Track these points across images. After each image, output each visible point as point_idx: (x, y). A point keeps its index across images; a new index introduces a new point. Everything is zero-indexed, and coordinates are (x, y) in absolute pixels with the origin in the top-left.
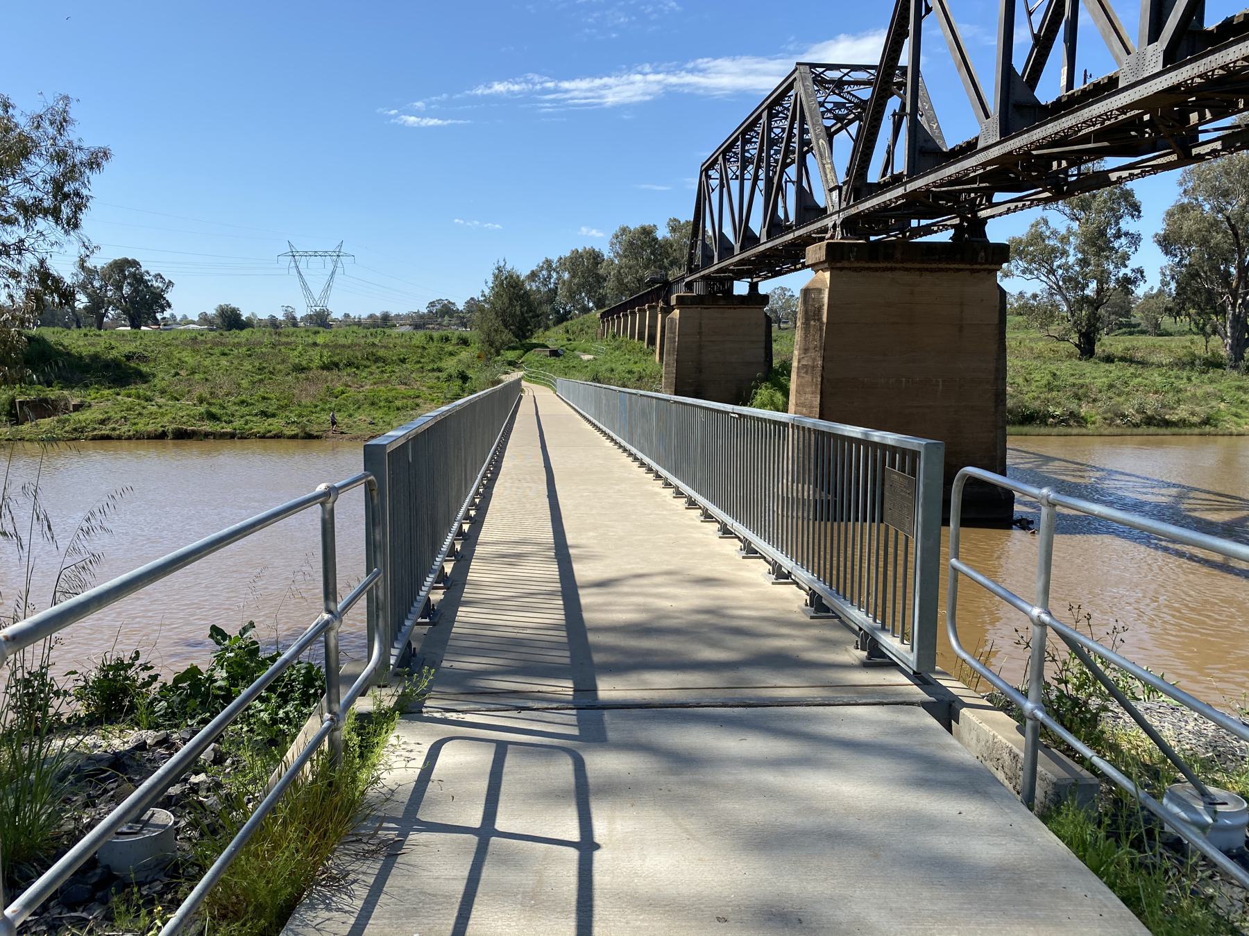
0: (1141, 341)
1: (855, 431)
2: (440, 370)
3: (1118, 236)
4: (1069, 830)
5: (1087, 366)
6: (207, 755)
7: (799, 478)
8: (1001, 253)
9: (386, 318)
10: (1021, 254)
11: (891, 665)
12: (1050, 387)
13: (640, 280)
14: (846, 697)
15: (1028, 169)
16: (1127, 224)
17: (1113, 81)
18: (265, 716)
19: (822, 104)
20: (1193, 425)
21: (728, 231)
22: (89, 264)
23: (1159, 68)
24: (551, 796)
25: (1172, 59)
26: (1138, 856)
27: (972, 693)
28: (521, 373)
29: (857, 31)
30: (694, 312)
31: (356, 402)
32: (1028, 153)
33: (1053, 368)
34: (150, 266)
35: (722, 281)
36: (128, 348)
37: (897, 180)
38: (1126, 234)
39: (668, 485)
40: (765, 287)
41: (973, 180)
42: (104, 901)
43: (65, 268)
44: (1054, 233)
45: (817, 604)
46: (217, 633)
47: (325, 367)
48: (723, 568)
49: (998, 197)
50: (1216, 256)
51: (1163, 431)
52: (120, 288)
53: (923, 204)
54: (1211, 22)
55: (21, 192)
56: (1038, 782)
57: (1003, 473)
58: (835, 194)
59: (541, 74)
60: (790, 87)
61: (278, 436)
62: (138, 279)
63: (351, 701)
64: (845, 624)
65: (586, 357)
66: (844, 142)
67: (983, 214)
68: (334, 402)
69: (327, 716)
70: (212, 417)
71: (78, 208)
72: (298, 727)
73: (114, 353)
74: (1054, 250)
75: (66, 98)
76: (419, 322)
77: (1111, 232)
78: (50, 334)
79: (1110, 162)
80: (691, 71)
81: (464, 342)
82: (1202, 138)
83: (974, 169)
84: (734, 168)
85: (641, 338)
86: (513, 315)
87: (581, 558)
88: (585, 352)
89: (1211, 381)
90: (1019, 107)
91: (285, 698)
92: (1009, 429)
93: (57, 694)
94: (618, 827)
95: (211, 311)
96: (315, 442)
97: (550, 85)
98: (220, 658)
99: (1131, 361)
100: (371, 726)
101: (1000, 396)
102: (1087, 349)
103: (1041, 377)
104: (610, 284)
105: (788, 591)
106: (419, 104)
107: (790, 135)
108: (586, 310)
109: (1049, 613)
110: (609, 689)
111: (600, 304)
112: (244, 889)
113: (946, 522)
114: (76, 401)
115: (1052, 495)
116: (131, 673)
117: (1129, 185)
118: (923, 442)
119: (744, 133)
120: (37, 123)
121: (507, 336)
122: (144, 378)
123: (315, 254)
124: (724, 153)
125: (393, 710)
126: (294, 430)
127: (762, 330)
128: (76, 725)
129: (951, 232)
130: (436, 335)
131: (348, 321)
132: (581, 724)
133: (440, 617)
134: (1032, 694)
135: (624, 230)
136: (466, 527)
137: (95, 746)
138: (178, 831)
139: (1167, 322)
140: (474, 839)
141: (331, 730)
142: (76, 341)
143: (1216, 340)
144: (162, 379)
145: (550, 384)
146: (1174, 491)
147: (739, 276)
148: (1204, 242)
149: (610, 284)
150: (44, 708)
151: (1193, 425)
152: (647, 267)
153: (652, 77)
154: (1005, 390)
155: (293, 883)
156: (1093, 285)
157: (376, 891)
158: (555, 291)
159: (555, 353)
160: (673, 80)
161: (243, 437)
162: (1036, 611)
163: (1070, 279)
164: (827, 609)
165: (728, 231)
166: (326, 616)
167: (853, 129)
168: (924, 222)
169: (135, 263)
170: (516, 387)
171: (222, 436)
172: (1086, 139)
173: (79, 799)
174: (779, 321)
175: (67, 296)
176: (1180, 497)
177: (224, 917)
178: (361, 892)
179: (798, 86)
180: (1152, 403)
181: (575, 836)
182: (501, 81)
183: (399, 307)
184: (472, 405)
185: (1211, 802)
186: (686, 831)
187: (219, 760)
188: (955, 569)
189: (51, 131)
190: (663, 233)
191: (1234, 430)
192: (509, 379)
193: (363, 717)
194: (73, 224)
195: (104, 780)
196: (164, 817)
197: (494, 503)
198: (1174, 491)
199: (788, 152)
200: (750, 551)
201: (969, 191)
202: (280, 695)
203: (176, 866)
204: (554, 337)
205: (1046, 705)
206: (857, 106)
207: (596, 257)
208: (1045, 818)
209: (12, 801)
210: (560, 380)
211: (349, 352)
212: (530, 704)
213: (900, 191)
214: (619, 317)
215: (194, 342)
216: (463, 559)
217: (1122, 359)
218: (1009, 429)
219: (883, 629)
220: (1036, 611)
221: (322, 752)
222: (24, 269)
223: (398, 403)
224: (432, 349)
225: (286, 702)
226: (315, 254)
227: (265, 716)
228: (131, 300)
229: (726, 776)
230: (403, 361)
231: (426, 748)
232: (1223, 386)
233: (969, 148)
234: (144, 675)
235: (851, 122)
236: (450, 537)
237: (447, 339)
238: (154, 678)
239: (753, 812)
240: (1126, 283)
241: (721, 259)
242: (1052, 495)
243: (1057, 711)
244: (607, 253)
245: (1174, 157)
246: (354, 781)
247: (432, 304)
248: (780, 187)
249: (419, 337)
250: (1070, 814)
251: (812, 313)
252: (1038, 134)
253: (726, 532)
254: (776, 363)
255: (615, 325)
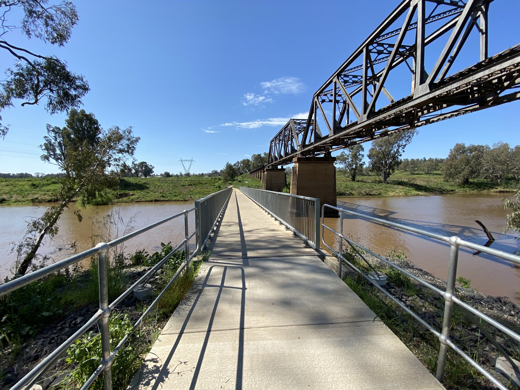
0: (365, 177)
1: (302, 197)
2: (214, 185)
3: (359, 155)
4: (348, 282)
5: (353, 183)
6: (159, 271)
7: (292, 207)
8: (334, 159)
9: (202, 174)
10: (339, 159)
11: (311, 247)
12: (346, 187)
13: (258, 166)
14: (301, 254)
15: (340, 141)
16: (361, 153)
17: (357, 122)
18: (173, 263)
19: (296, 128)
20: (376, 195)
21: (276, 155)
22: (135, 163)
23: (366, 120)
24: (236, 278)
25: (369, 118)
26: (363, 287)
27: (328, 253)
28: (232, 186)
29: (303, 112)
30: (269, 172)
31: (196, 193)
32: (339, 138)
33: (346, 183)
34: (149, 163)
35: (275, 165)
36: (144, 182)
37: (312, 144)
38: (361, 155)
39: (264, 209)
40: (285, 167)
41: (328, 144)
42: (135, 305)
43: (129, 164)
44: (346, 154)
45: (295, 234)
46: (163, 244)
47: (189, 185)
48: (276, 227)
49: (334, 147)
50: (380, 159)
51: (370, 196)
52: (142, 168)
53: (317, 149)
54: (376, 110)
55: (120, 147)
56: (342, 272)
57: (336, 206)
58: (299, 147)
59: (236, 122)
60: (289, 124)
61: (178, 201)
62: (146, 166)
63: (192, 258)
64: (301, 239)
65: (246, 182)
66: (301, 136)
67: (330, 151)
68: (191, 193)
69: (186, 261)
70: (163, 197)
71: (133, 151)
72: (180, 265)
73: (141, 183)
74: (346, 158)
75: (131, 127)
76: (210, 175)
77: (358, 154)
78: (126, 179)
79: (357, 139)
80: (268, 121)
81: (220, 179)
82: (376, 134)
83: (328, 141)
84: (277, 142)
85: (258, 178)
86: (231, 173)
87: (245, 225)
88: (246, 181)
89: (380, 186)
90: (337, 128)
91: (178, 259)
92: (337, 197)
93: (126, 259)
94: (251, 284)
95: (163, 173)
96: (186, 202)
97: (238, 124)
98: (163, 250)
99: (363, 182)
100: (196, 264)
101: (335, 189)
102: (353, 179)
103: (344, 185)
104: (251, 166)
105: (289, 232)
106: (209, 128)
107: (289, 135)
108: (246, 172)
109: (343, 235)
110: (250, 254)
111: (249, 171)
112: (167, 301)
113: (321, 217)
114: (132, 194)
115: (342, 210)
116: (143, 254)
117: (361, 144)
118: (316, 199)
119: (279, 134)
120: (124, 132)
121: (229, 178)
122: (148, 188)
123: (187, 160)
124: (275, 138)
125: (201, 260)
126: (182, 199)
127: (284, 176)
128: (130, 266)
129: (324, 155)
130: (213, 178)
131: (194, 175)
132: (243, 262)
133: (213, 240)
134: (340, 253)
135: (254, 155)
136: (219, 220)
137: (134, 270)
138: (152, 289)
139: (370, 173)
140: (219, 288)
141: (187, 264)
142: (132, 180)
143: (380, 177)
144: (152, 188)
145: (238, 188)
146: (373, 209)
147: (279, 164)
148: (377, 156)
149: (251, 166)
150: (123, 263)
151: (376, 195)
152: (259, 163)
153: (260, 122)
154: (336, 189)
155: (178, 299)
156: (354, 166)
157: (196, 300)
158: (239, 168)
159: (239, 181)
160: (264, 123)
161: (170, 201)
162: (340, 235)
163: (349, 164)
164: (297, 236)
165: (276, 155)
166: (186, 239)
167: (303, 133)
168: (318, 153)
169: (145, 163)
170: (231, 189)
171: (165, 201)
172: (351, 135)
173: (130, 282)
174: (288, 174)
175: (130, 170)
176: (374, 210)
177: (162, 308)
178: (193, 301)
179: (291, 124)
180: (368, 190)
181: (241, 286)
182: (227, 123)
183: (205, 172)
184: (220, 193)
185: (378, 275)
186: (266, 284)
187: (162, 273)
188: (323, 226)
189: (127, 134)
190: (263, 155)
191: (385, 196)
192: (229, 187)
193: (195, 262)
194: (132, 153)
195: (136, 278)
196: (149, 285)
197: (226, 214)
198: (373, 209)
199: (289, 138)
200: (281, 223)
201: (327, 146)
202: (177, 258)
203: (151, 296)
204: (239, 178)
205: (343, 255)
206: (303, 128)
207: (248, 161)
208: (343, 280)
209: (114, 283)
210: (241, 187)
211: (194, 182)
212: (232, 258)
213: (312, 146)
214: (258, 172)
215: (159, 180)
216: (218, 227)
217: (361, 181)
218: (337, 197)
219: (309, 239)
220: (340, 235)
221: (185, 270)
222: (120, 164)
223: (205, 193)
224: (213, 181)
225: (178, 259)
226: (187, 160)
227: (173, 263)
228: (145, 171)
229: (275, 272)
230: (206, 184)
231: (209, 268)
232: (382, 186)
233: (327, 137)
234: (146, 254)
235: (302, 131)
236: (216, 221)
237: (216, 179)
238: (148, 255)
239: (280, 280)
240: (361, 165)
241: (275, 161)
242: (342, 210)
243: (346, 256)
244: (251, 160)
245: (370, 138)
246: (193, 276)
247: (213, 171)
248: (287, 145)
249: (210, 178)
250: (349, 279)
251: (294, 172)
252: (341, 134)
253: (276, 219)
254: (287, 183)
255: (254, 175)
